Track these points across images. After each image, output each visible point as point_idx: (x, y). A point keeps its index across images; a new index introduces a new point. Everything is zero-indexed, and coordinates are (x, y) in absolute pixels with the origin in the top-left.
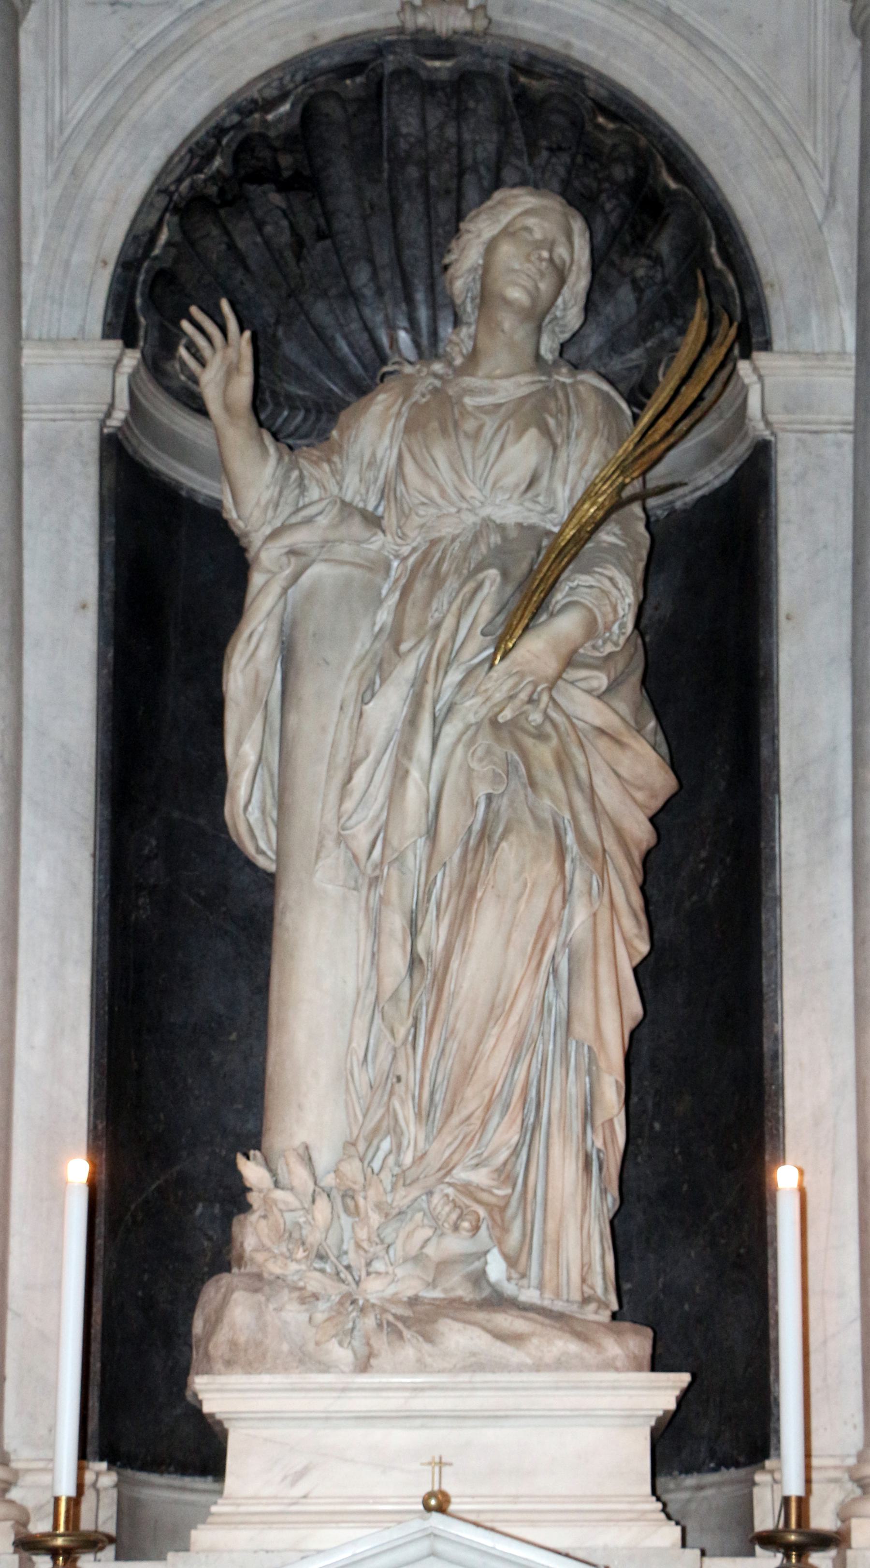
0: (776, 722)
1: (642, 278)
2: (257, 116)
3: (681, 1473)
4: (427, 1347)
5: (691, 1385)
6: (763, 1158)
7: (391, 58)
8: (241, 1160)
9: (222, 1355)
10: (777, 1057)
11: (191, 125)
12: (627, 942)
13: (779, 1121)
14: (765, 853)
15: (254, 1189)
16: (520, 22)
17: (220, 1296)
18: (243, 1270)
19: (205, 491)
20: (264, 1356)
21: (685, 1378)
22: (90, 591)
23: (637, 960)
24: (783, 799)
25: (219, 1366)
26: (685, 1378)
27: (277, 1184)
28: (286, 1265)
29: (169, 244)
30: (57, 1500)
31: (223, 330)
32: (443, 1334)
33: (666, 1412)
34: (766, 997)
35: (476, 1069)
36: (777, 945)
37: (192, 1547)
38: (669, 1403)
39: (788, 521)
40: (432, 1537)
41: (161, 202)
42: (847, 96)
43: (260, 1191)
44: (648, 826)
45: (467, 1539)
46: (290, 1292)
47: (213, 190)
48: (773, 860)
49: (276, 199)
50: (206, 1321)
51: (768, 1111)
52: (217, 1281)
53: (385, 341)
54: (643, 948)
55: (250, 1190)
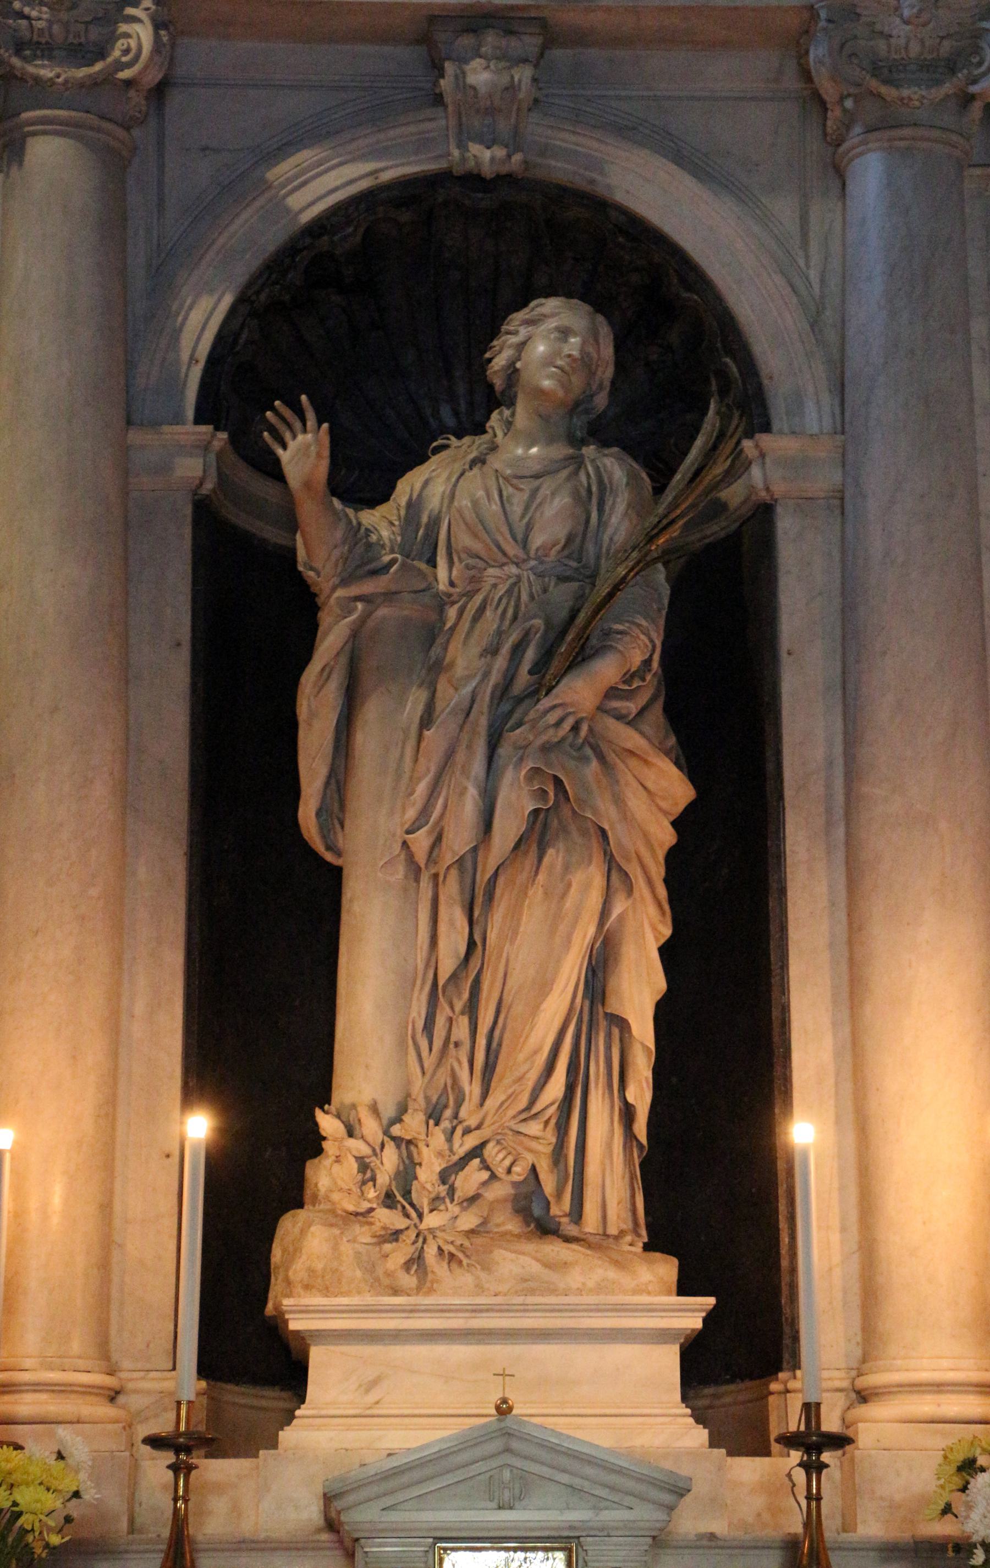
2: (326, 238)
3: (700, 1384)
4: (483, 1275)
5: (715, 1307)
7: (441, 191)
10: (785, 1024)
11: (271, 248)
15: (330, 1138)
20: (339, 1281)
21: (711, 1301)
23: (662, 941)
24: (786, 805)
25: (299, 1290)
26: (711, 1301)
27: (351, 1134)
31: (304, 425)
32: (498, 1263)
33: (693, 1330)
34: (774, 974)
35: (527, 1037)
36: (783, 929)
37: (280, 1446)
38: (695, 1322)
39: (789, 572)
40: (507, 1436)
43: (335, 1140)
45: (428, 1455)
46: (361, 1226)
48: (780, 857)
50: (284, 1251)
51: (778, 1071)
53: (428, 411)
54: (667, 932)
55: (324, 1138)
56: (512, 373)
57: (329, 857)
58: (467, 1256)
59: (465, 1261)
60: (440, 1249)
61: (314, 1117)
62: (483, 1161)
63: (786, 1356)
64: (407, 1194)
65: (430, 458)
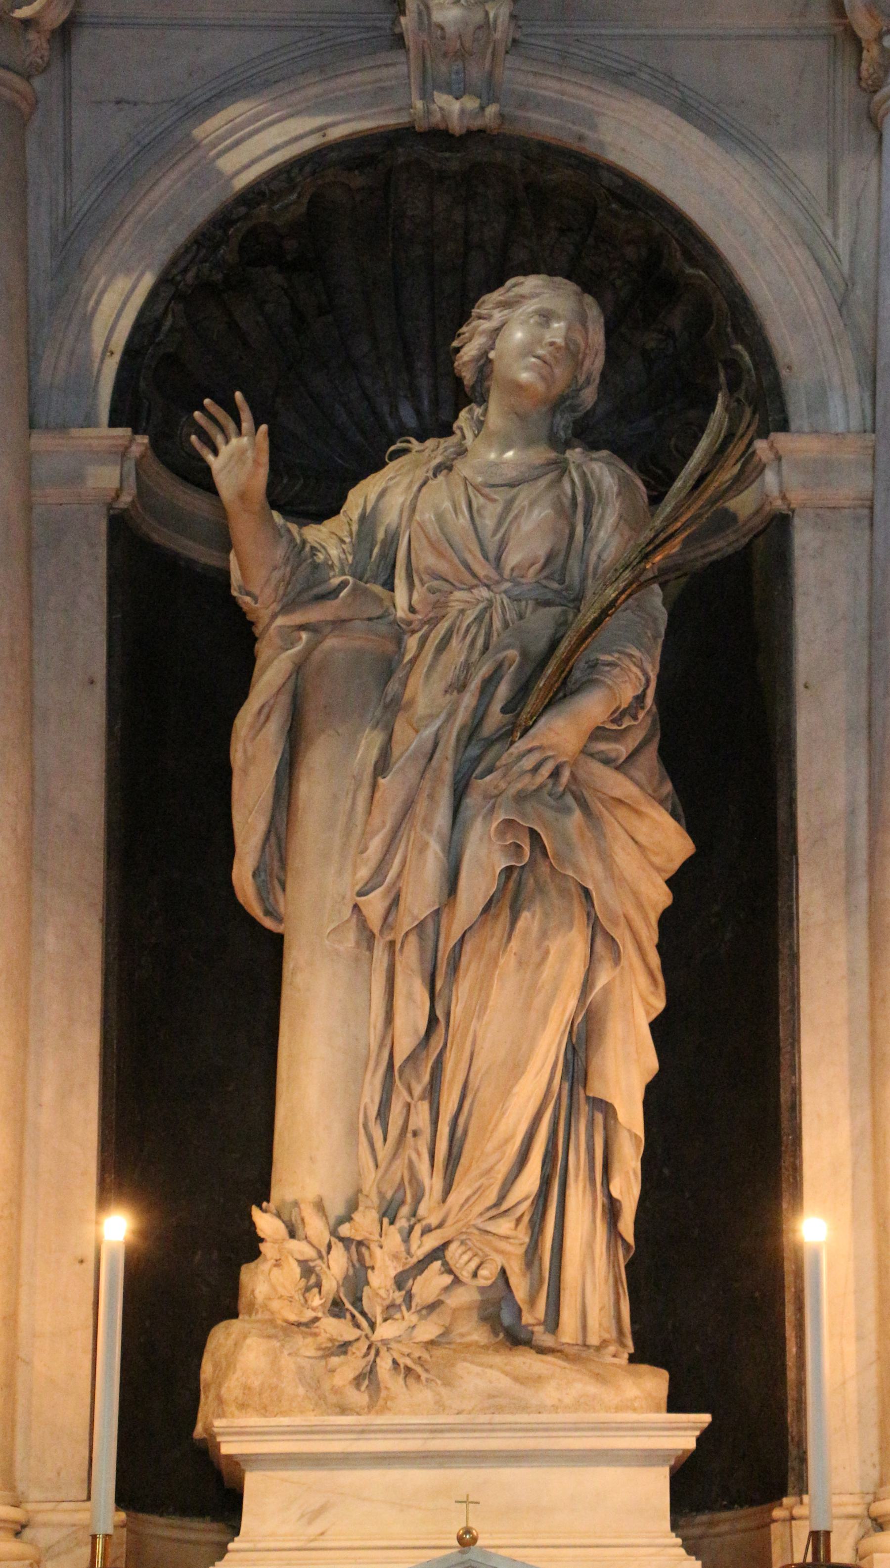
0: (792, 784)
1: (652, 350)
2: (264, 207)
4: (443, 1391)
5: (711, 1425)
6: (779, 1205)
7: (400, 150)
8: (256, 1213)
9: (236, 1398)
10: (795, 1108)
12: (643, 999)
13: (797, 1169)
14: (783, 911)
15: (268, 1239)
16: (534, 115)
17: (230, 1342)
18: (253, 1317)
19: (203, 560)
22: (99, 668)
23: (654, 1015)
24: (800, 860)
25: (232, 1408)
26: (706, 1418)
27: (292, 1234)
28: (301, 1312)
29: (172, 329)
30: (94, 1537)
31: (238, 423)
33: (684, 1451)
35: (496, 1125)
36: (795, 1000)
41: (167, 292)
42: (866, 184)
44: (666, 888)
46: (304, 1337)
47: (218, 277)
48: (792, 919)
49: (278, 278)
52: (227, 1328)
55: (262, 1240)
56: (484, 365)
57: (268, 923)
58: (427, 1370)
59: (424, 1376)
60: (395, 1362)
61: (250, 1216)
62: (445, 1264)
63: (792, 1479)
64: (357, 1301)
65: (387, 464)
